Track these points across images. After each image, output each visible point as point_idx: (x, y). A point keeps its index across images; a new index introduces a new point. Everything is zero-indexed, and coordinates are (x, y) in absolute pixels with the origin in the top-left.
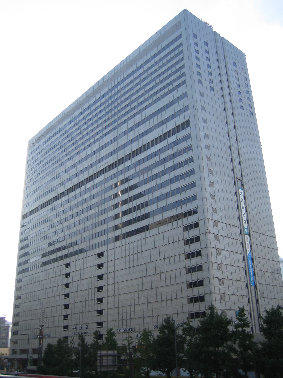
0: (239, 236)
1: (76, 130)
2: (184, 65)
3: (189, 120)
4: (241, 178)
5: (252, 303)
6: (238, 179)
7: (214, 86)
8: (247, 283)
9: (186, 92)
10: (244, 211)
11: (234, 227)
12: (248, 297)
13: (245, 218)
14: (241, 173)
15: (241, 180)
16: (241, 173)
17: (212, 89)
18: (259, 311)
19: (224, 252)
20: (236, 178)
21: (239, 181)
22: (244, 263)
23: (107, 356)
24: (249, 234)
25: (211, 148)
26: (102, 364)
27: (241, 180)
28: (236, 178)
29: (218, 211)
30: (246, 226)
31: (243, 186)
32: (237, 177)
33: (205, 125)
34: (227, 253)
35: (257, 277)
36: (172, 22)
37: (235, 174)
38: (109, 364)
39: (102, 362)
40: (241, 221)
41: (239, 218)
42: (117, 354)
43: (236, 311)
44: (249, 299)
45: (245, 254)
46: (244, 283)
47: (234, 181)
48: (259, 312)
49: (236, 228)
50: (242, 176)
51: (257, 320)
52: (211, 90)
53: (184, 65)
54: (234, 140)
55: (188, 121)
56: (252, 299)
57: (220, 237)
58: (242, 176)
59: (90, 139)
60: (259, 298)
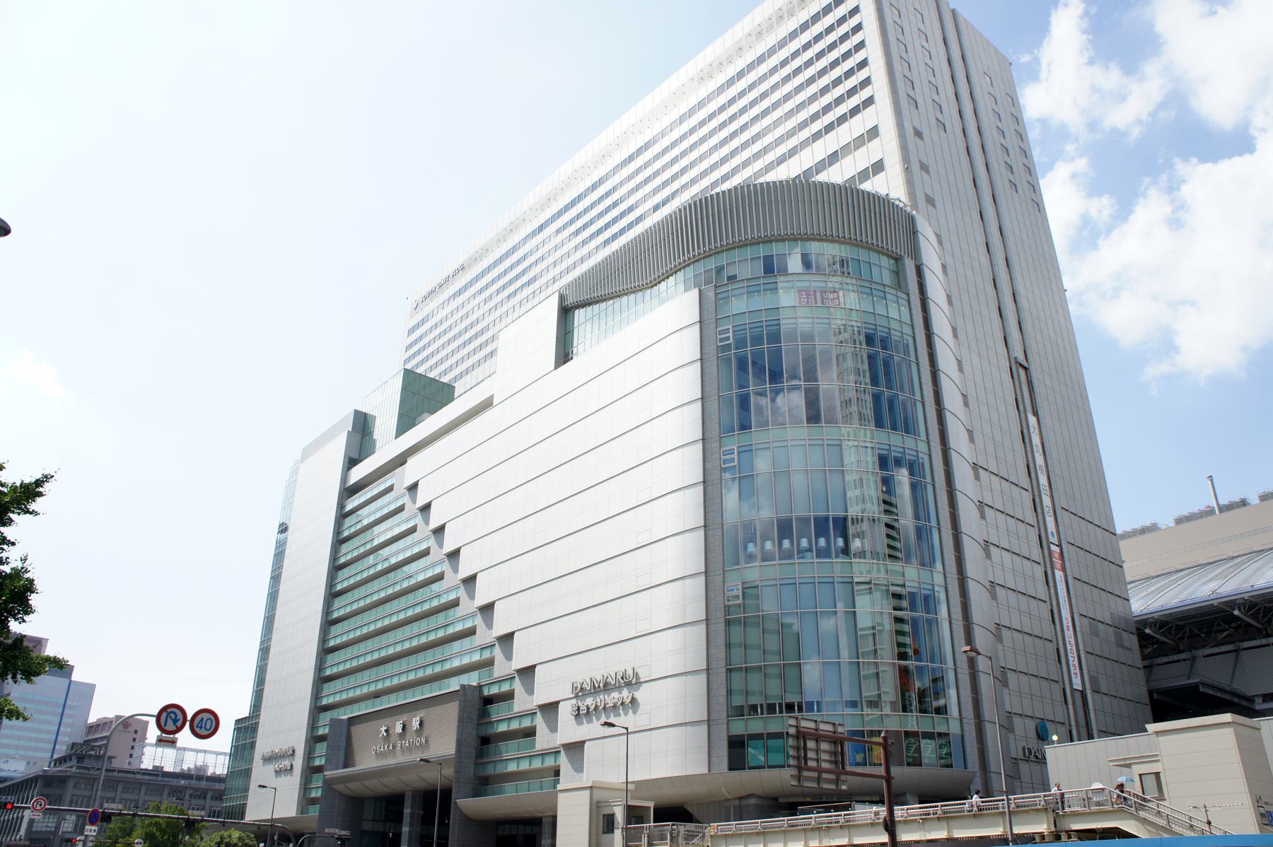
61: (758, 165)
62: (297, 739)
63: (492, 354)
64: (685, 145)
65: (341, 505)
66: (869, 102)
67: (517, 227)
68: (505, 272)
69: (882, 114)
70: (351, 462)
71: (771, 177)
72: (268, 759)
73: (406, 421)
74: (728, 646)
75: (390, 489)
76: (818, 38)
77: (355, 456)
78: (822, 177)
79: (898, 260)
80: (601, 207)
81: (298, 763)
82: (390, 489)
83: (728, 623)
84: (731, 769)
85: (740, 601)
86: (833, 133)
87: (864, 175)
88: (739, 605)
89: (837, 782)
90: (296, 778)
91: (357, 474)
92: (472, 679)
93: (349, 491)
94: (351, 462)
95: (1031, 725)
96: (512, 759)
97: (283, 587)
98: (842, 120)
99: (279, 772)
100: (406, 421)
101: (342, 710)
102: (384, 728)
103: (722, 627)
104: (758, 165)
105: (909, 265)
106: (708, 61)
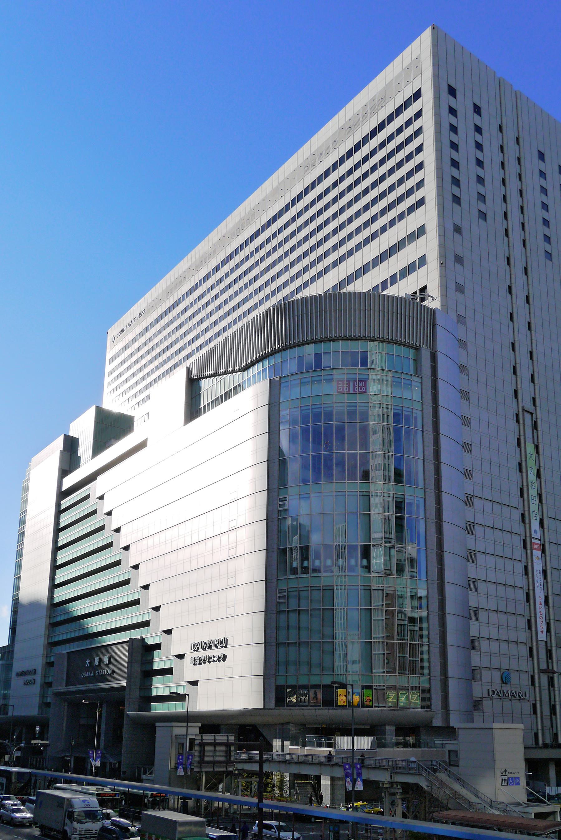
0: (519, 553)
1: (157, 345)
2: (421, 128)
3: (425, 288)
4: (532, 409)
5: (538, 658)
6: (526, 411)
7: (488, 208)
8: (526, 564)
9: (423, 198)
10: (532, 477)
11: (508, 509)
12: (526, 590)
13: (533, 493)
14: (534, 399)
15: (532, 414)
16: (534, 399)
17: (483, 215)
18: (552, 699)
19: (483, 556)
20: (520, 410)
21: (528, 417)
22: (530, 663)
23: (215, 744)
24: (543, 549)
25: (470, 347)
26: (204, 758)
27: (532, 414)
28: (520, 410)
29: (476, 476)
30: (534, 507)
31: (535, 425)
32: (523, 407)
33: (460, 296)
34: (491, 559)
35: (540, 432)
36: (384, 341)
37: (520, 400)
38: (218, 759)
39: (204, 756)
40: (525, 496)
41: (522, 490)
42: (233, 742)
43: (503, 671)
44: (531, 649)
45: (530, 562)
46: (520, 564)
47: (517, 415)
48: (549, 648)
49: (514, 510)
50: (534, 404)
51: (547, 692)
52: (479, 217)
53: (421, 128)
54: (521, 272)
55: (423, 227)
56: (536, 621)
57: (477, 528)
58: (534, 404)
59: (199, 311)
60: (554, 648)
61: (293, 287)
62: (38, 664)
63: (147, 398)
64: (231, 278)
65: (58, 505)
66: (421, 202)
67: (180, 283)
68: (275, 235)
69: (428, 216)
70: (64, 472)
71: (306, 293)
72: (21, 674)
73: (100, 446)
74: (278, 628)
75: (87, 497)
76: (306, 209)
77: (66, 468)
78: (350, 288)
79: (417, 349)
80: (300, 221)
81: (38, 678)
82: (87, 497)
83: (279, 612)
84: (276, 706)
85: (286, 600)
86: (413, 215)
87: (384, 285)
88: (285, 602)
89: (214, 756)
90: (36, 689)
91: (69, 481)
92: (136, 634)
93: (62, 494)
94: (64, 472)
95: (497, 675)
96: (160, 687)
97: (25, 558)
98: (358, 247)
99: (27, 683)
100: (100, 446)
101: (63, 647)
102: (88, 661)
103: (274, 616)
104: (293, 287)
105: (426, 354)
106: (356, 111)
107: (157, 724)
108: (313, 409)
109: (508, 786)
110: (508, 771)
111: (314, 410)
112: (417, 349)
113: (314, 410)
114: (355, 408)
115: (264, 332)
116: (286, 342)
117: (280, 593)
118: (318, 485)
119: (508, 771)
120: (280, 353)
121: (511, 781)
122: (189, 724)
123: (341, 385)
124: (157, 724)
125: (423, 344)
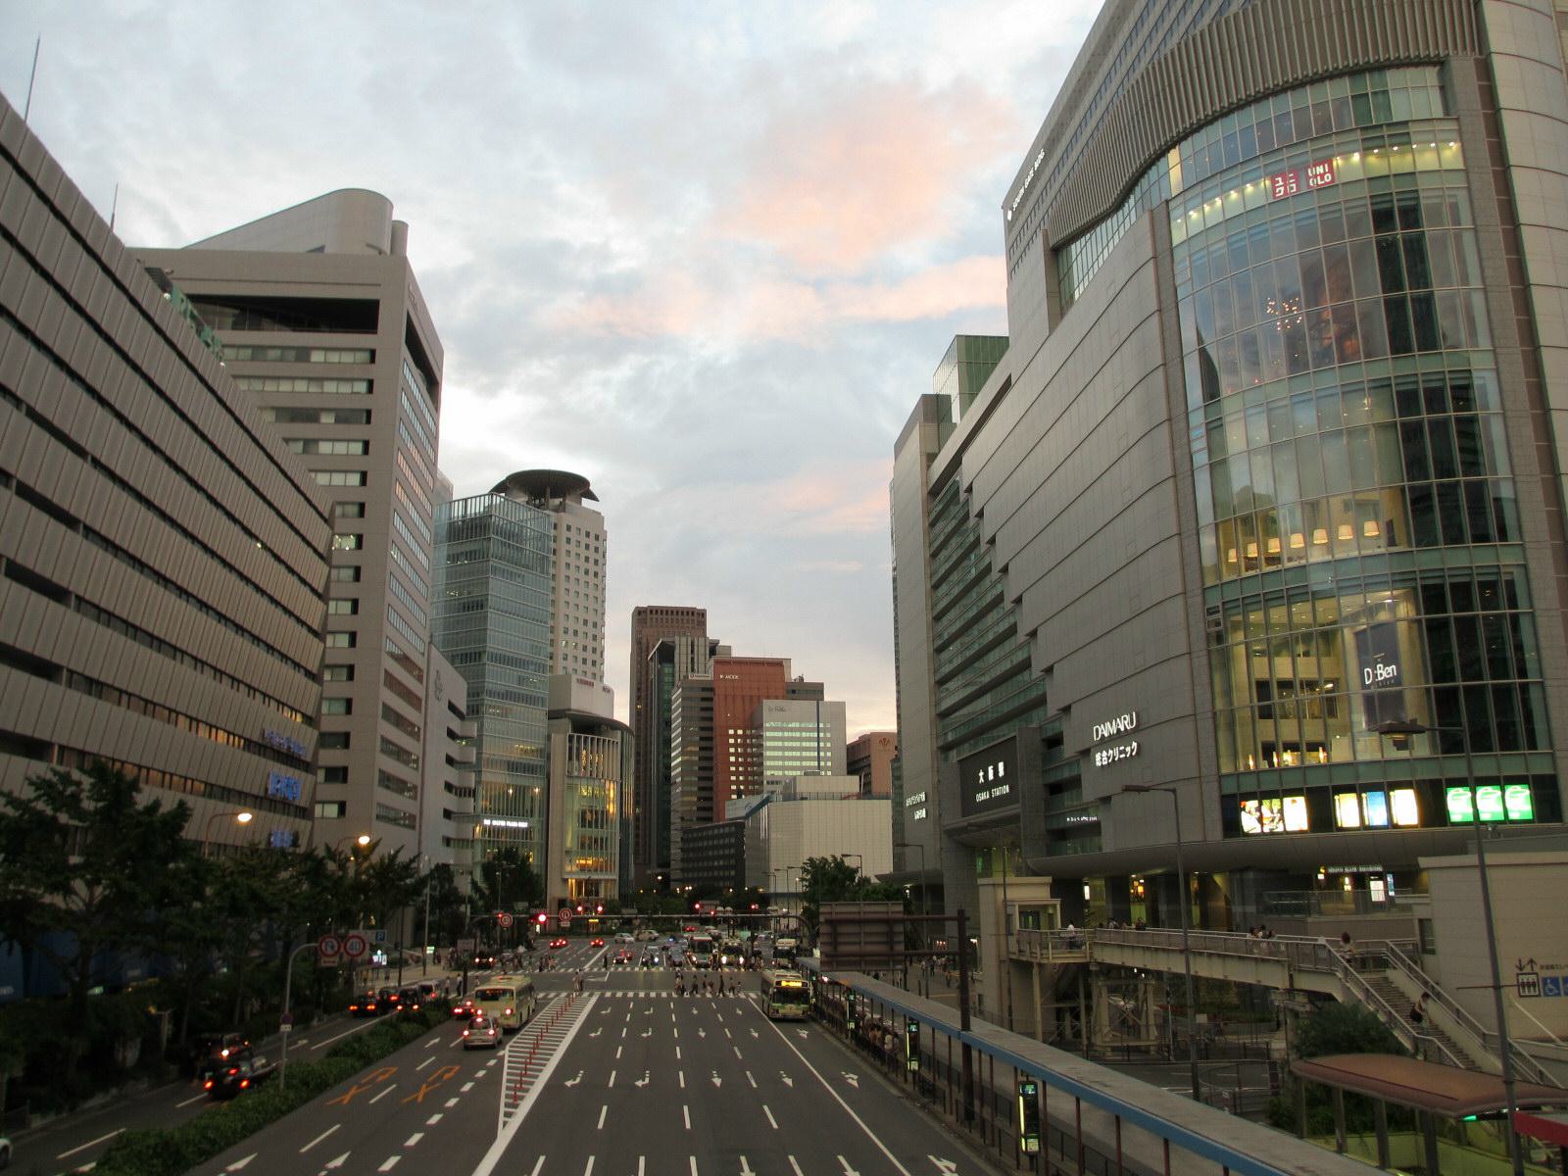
42: (901, 916)
105: (1463, 68)
107: (1423, 862)
108: (1297, 221)
109: (1543, 999)
110: (1540, 961)
111: (1351, 212)
112: (1440, 63)
113: (1351, 212)
114: (1337, 215)
115: (1165, 99)
116: (1354, 58)
117: (1211, 614)
118: (1411, 359)
119: (1540, 961)
120: (1190, 139)
121: (1550, 986)
122: (1489, 859)
123: (1281, 183)
124: (1423, 862)
125: (1456, 47)
